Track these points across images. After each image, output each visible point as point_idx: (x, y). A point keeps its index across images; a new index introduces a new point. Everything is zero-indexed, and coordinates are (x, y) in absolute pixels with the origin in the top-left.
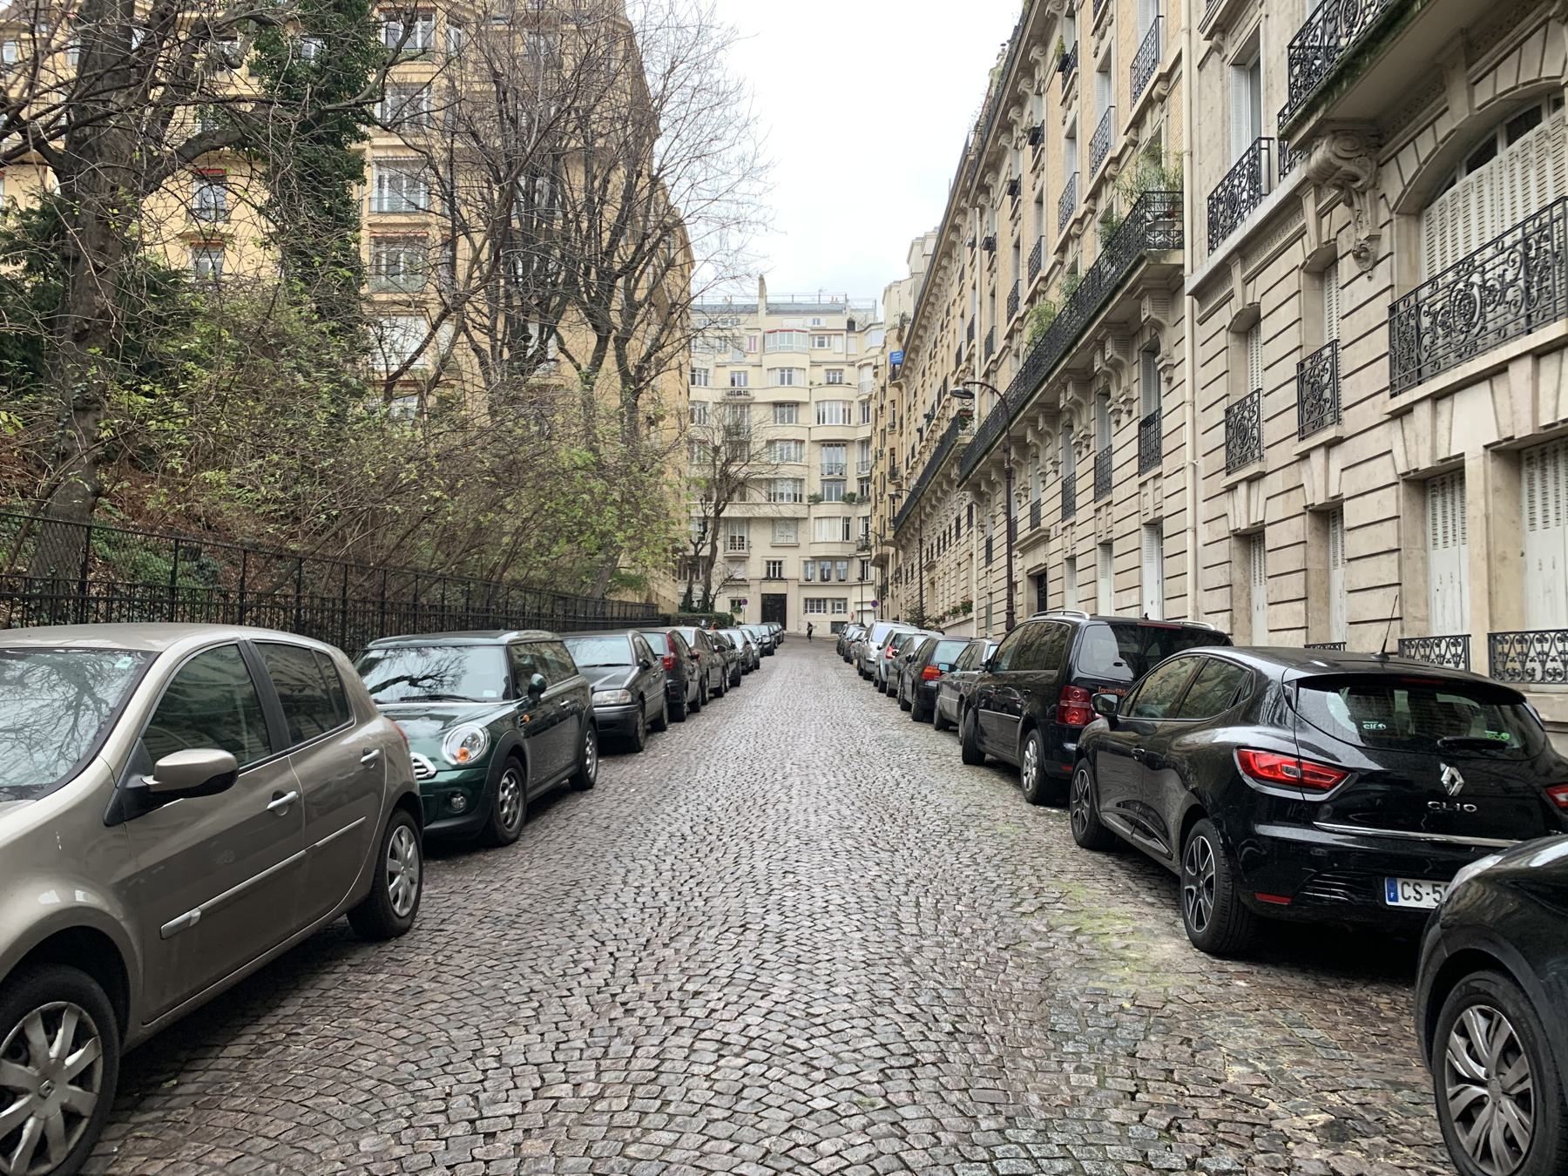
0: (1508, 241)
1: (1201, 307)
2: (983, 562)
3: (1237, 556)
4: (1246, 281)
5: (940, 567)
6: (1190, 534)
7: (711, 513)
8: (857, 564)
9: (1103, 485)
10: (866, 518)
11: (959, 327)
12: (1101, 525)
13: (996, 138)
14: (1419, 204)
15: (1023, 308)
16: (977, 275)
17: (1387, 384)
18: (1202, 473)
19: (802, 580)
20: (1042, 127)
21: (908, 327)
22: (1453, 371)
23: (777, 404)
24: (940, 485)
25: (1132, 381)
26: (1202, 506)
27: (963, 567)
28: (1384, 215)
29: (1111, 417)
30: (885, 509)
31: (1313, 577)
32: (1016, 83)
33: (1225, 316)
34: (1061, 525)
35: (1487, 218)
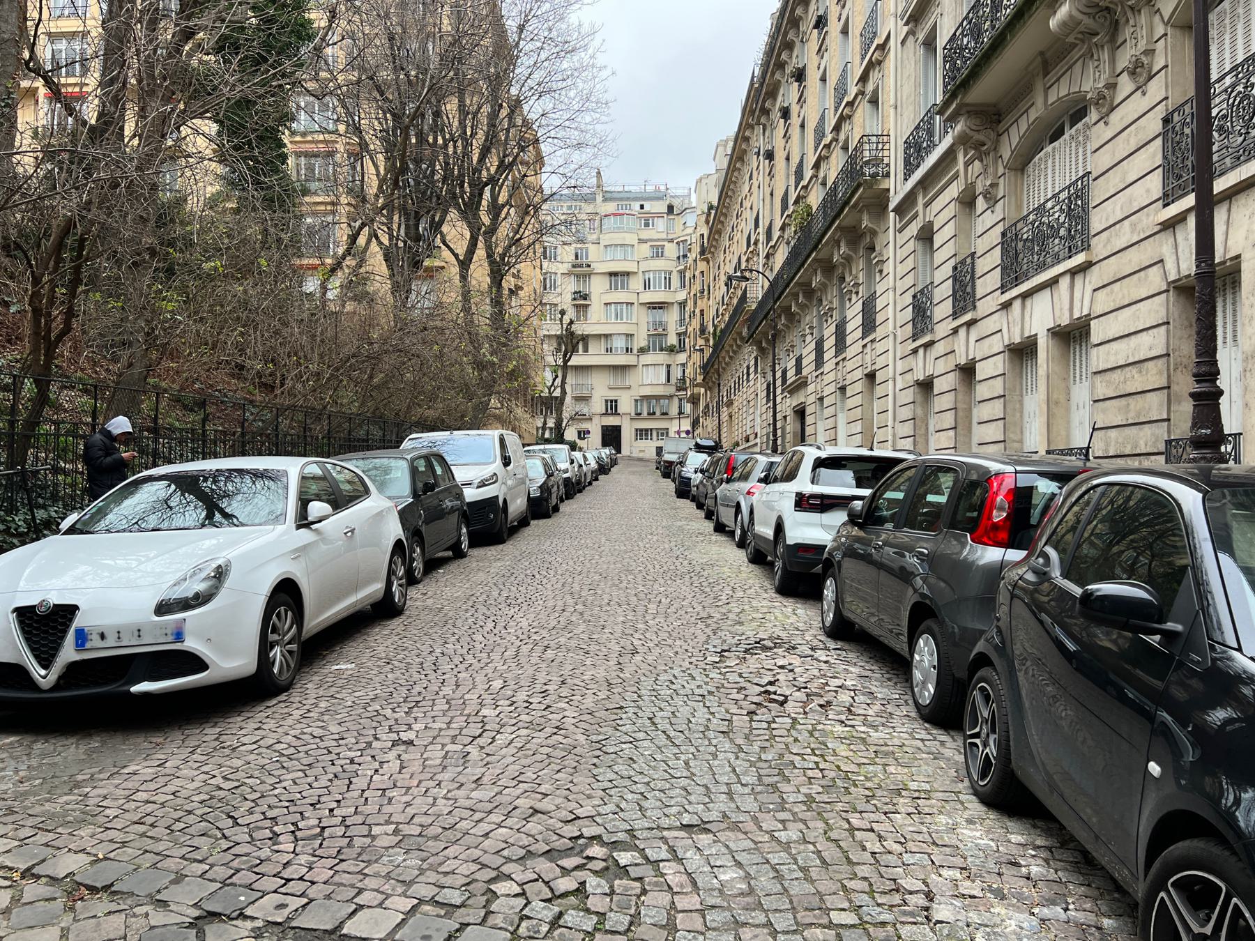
0: (1062, 196)
1: (900, 221)
2: (764, 401)
3: (919, 398)
4: (926, 205)
6: (890, 382)
7: (560, 362)
8: (676, 400)
9: (841, 345)
10: (683, 365)
11: (749, 216)
12: (868, 358)
13: (773, 74)
14: (1021, 164)
16: (760, 178)
17: (1161, 194)
18: (899, 340)
20: (804, 67)
21: (713, 212)
23: (611, 274)
24: (735, 340)
25: (859, 271)
26: (899, 363)
27: (752, 403)
28: (1001, 170)
29: (844, 297)
30: (696, 357)
31: (960, 414)
32: (786, 33)
33: (913, 229)
34: (815, 374)
35: (1057, 178)
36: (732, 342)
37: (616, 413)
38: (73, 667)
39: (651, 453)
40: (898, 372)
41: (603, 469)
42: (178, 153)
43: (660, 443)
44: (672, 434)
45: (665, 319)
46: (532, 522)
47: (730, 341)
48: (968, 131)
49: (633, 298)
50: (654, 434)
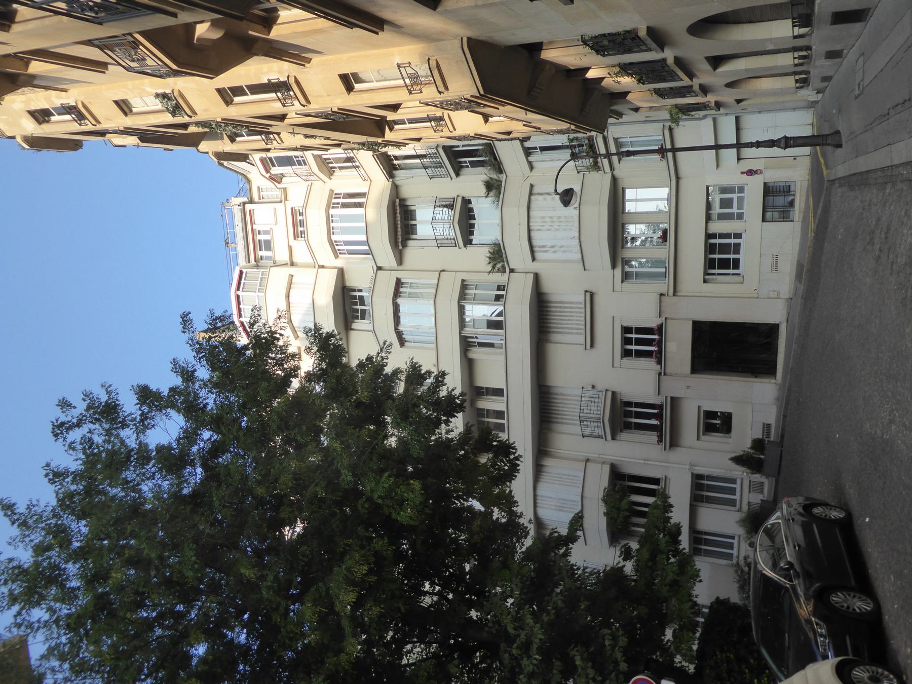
42: (235, 546)
50: (717, 227)
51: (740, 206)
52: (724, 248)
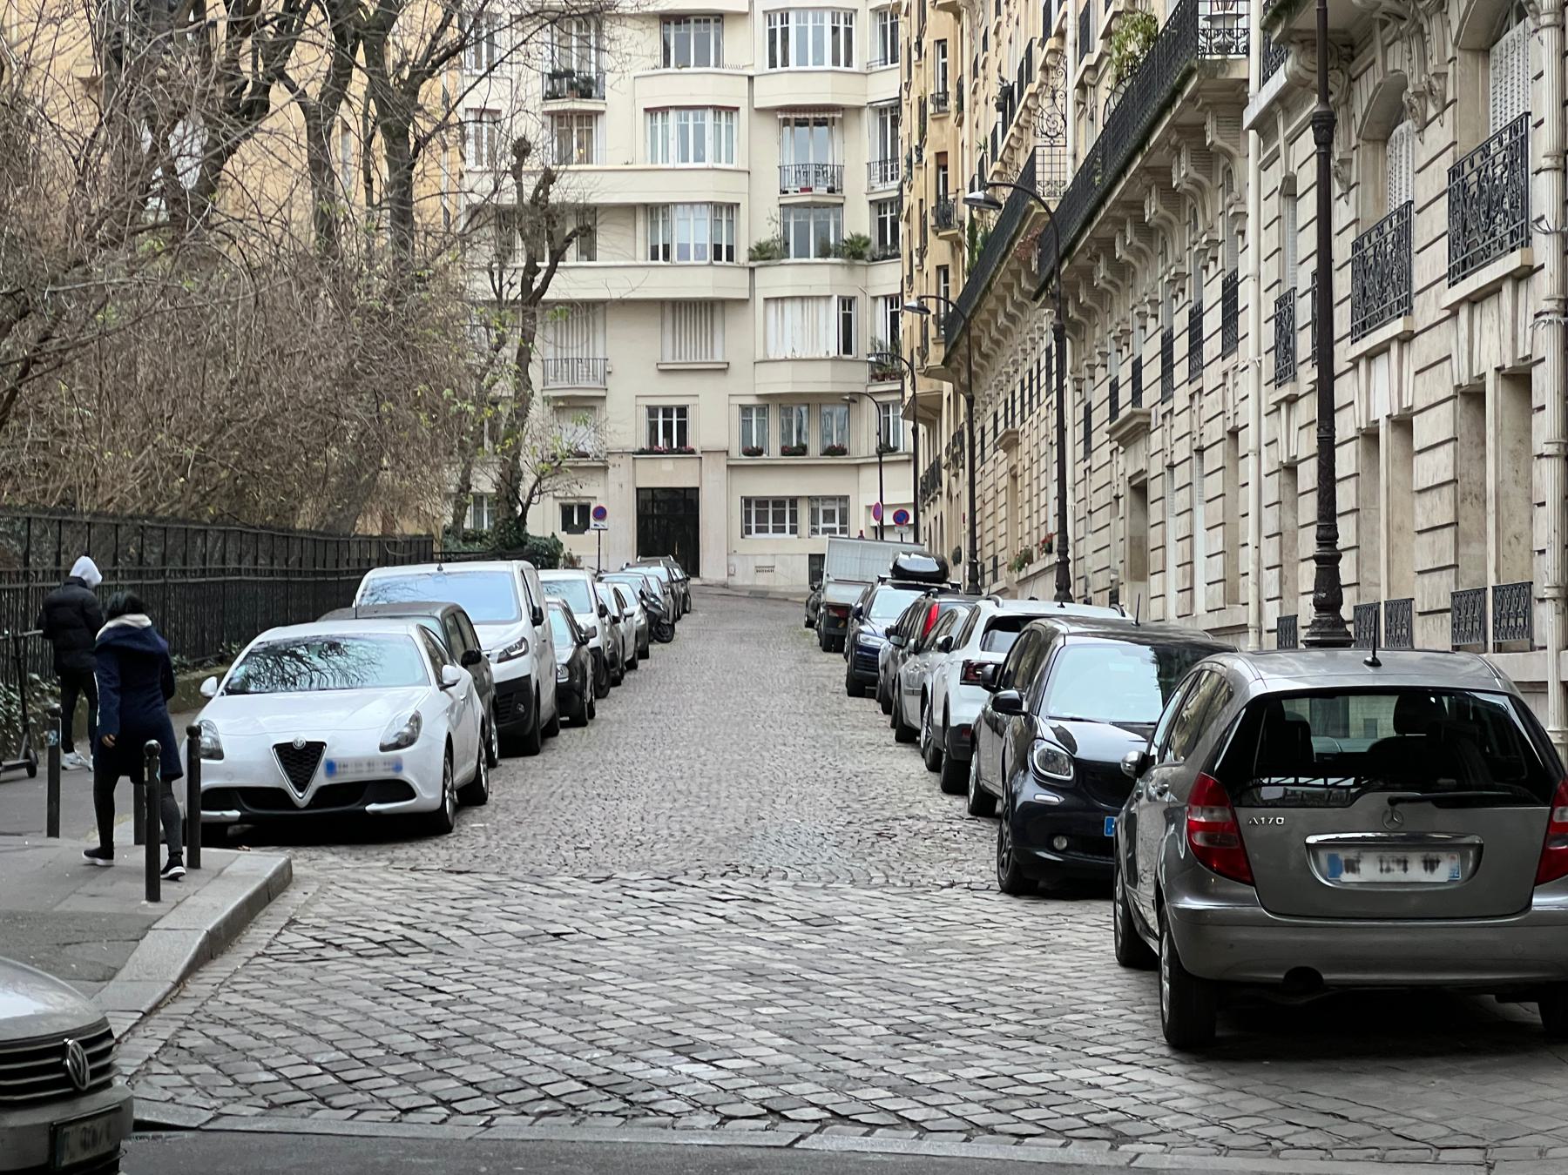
5: (1025, 445)
8: (869, 410)
10: (893, 300)
15: (1098, 45)
19: (736, 452)
22: (1499, 262)
36: (1008, 278)
37: (683, 449)
38: (322, 791)
39: (795, 577)
40: (1264, 442)
41: (659, 629)
43: (820, 544)
44: (861, 521)
45: (834, 156)
46: (562, 732)
47: (1003, 275)
48: (1302, 72)
49: (733, 93)
50: (804, 513)
51: (825, 531)
52: (779, 517)
